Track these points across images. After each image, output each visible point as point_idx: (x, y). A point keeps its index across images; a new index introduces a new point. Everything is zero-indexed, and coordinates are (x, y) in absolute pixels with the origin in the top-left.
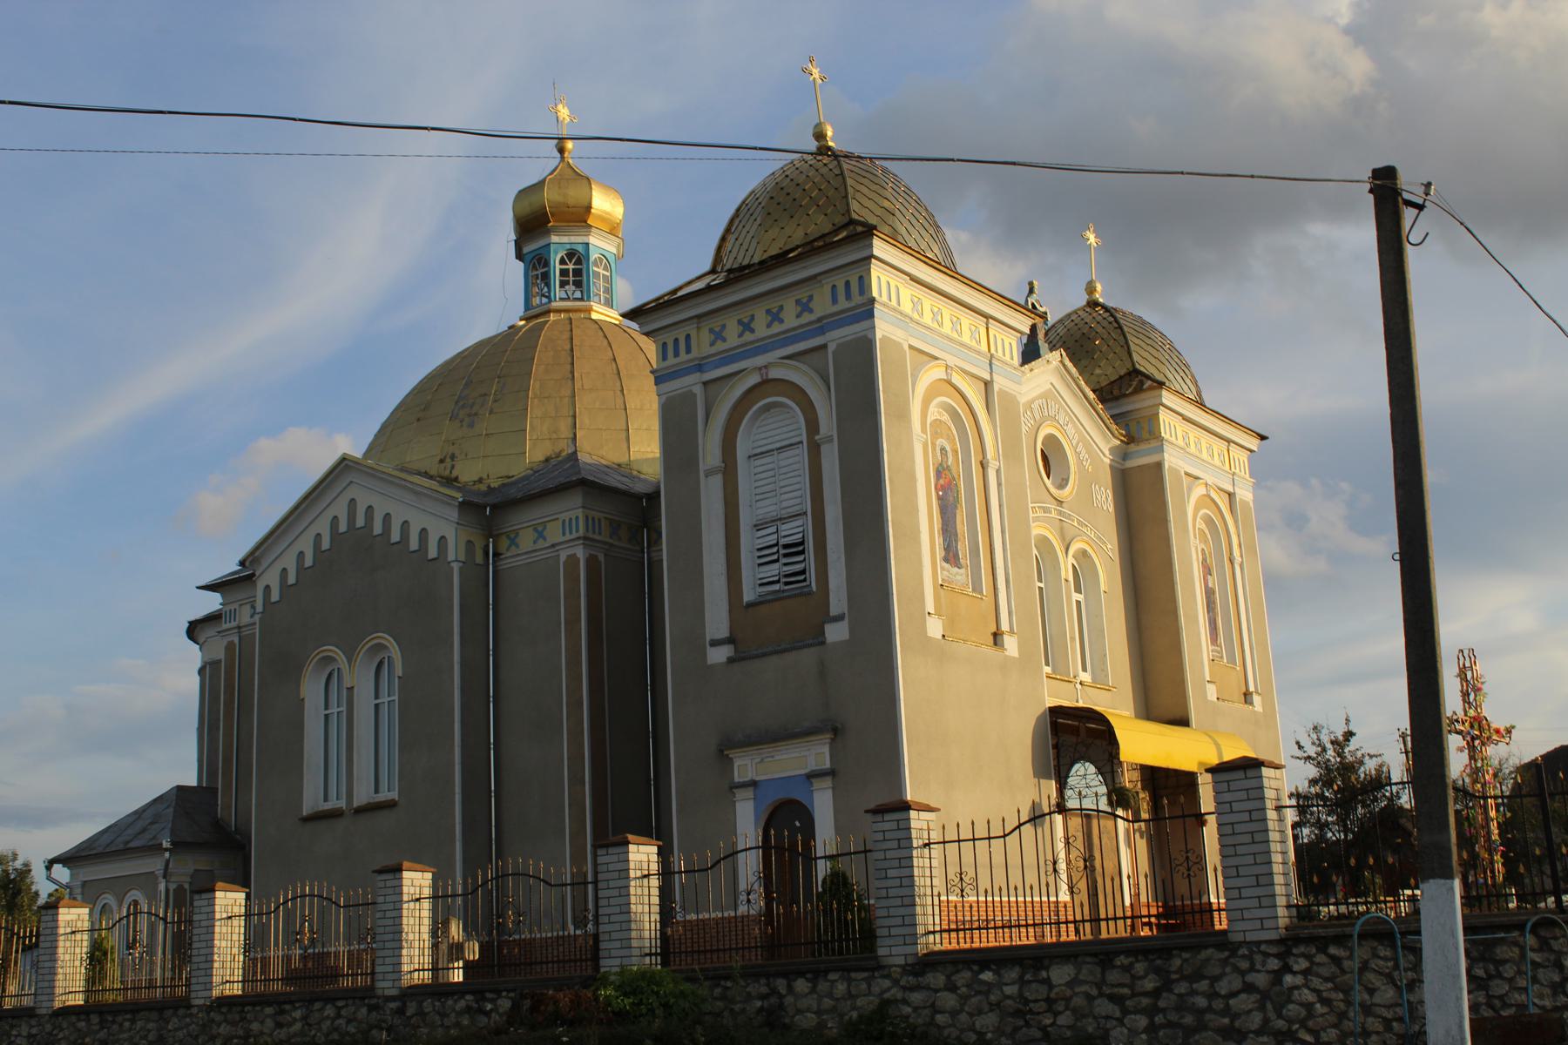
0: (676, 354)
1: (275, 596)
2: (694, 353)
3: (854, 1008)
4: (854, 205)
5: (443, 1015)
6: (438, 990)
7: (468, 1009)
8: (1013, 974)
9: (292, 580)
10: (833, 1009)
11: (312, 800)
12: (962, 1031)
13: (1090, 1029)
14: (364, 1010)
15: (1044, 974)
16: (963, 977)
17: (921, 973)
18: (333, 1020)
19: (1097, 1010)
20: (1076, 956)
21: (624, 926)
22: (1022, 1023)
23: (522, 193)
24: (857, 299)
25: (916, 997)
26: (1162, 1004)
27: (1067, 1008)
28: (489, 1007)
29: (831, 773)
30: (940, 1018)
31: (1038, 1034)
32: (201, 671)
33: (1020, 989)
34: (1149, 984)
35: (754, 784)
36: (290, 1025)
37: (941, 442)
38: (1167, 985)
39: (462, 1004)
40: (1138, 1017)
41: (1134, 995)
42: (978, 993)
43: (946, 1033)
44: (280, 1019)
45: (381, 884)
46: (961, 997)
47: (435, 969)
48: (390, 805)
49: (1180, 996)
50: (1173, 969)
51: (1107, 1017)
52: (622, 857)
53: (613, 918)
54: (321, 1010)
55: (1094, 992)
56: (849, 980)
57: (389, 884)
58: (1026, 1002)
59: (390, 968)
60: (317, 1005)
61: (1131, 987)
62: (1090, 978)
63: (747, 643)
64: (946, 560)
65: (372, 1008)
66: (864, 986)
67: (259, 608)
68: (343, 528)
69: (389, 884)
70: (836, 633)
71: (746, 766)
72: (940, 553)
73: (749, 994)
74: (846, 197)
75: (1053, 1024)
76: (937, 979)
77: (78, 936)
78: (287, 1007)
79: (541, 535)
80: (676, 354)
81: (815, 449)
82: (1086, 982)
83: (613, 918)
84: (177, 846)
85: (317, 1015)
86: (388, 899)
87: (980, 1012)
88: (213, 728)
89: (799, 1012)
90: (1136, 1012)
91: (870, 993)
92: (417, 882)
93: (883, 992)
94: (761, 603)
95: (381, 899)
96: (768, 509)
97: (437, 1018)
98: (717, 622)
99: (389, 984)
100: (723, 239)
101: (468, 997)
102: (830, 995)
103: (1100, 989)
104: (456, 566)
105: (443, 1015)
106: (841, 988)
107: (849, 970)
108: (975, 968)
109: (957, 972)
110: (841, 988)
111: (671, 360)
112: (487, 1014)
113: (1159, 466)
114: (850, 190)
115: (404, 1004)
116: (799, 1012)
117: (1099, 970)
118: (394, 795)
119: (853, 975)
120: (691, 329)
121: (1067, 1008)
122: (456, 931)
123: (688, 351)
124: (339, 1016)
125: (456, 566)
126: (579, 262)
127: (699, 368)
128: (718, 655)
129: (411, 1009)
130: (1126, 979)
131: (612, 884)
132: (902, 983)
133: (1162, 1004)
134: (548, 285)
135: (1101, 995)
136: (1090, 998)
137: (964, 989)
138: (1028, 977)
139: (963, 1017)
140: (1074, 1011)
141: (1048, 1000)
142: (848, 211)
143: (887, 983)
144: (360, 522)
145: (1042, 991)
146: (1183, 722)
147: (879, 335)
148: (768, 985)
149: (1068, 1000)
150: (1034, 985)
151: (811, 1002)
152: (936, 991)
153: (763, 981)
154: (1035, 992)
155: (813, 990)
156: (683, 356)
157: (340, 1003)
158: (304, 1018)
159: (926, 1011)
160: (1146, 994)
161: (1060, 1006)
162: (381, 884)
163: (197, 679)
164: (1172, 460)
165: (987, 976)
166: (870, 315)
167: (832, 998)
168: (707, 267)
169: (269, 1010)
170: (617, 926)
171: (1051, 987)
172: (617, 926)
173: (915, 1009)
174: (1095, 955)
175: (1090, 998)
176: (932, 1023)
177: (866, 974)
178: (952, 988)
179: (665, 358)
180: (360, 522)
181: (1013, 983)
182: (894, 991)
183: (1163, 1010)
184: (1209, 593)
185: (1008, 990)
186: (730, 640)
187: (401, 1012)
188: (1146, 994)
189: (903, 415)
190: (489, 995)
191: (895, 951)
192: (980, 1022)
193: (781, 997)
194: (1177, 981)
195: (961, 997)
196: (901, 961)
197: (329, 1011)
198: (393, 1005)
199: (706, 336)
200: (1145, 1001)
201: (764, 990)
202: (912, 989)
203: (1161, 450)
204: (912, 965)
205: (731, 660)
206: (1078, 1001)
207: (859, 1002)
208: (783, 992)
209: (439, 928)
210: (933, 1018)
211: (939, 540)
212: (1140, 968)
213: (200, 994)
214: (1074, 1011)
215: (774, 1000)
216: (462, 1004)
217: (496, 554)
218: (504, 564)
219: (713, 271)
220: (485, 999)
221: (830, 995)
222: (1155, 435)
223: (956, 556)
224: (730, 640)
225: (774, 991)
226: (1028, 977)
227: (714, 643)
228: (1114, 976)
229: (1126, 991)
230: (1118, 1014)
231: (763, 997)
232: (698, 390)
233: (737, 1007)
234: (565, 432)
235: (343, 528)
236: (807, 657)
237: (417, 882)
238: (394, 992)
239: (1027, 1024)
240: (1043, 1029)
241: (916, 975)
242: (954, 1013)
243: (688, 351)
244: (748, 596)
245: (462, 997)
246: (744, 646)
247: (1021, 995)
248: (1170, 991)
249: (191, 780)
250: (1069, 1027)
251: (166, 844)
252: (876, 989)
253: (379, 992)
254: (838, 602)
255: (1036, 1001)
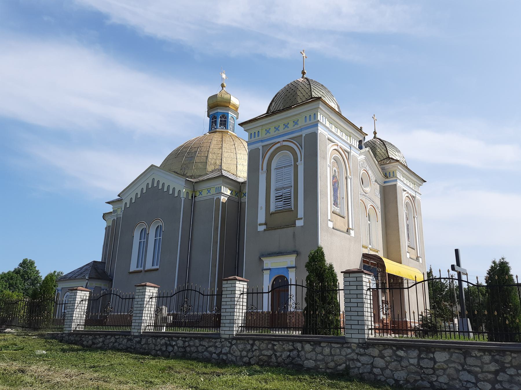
0: (255, 137)
1: (128, 206)
2: (260, 137)
3: (333, 361)
4: (313, 93)
5: (156, 345)
6: (155, 336)
7: (166, 344)
8: (415, 353)
9: (133, 201)
10: (323, 360)
11: (133, 268)
12: (387, 378)
13: (458, 386)
14: (125, 340)
15: (431, 355)
16: (388, 352)
17: (368, 348)
18: (114, 343)
19: (461, 378)
20: (449, 348)
21: (232, 314)
22: (419, 378)
23: (210, 99)
24: (313, 121)
25: (364, 359)
26: (499, 378)
27: (444, 374)
28: (174, 343)
29: (295, 267)
30: (375, 370)
31: (428, 385)
32: (106, 228)
33: (418, 362)
34: (493, 367)
35: (270, 269)
36: (98, 344)
37: (334, 168)
38: (503, 369)
39: (163, 341)
40: (486, 383)
41: (482, 372)
42: (395, 360)
43: (379, 378)
44: (94, 341)
45: (138, 291)
46: (386, 362)
47: (156, 326)
48: (157, 270)
49: (511, 376)
50: (507, 361)
51: (467, 382)
52: (233, 285)
53: (227, 310)
54: (110, 338)
55: (460, 368)
56: (331, 348)
57: (141, 291)
58: (422, 368)
59: (137, 324)
60: (109, 337)
61: (481, 368)
62: (457, 361)
63: (271, 226)
64: (334, 205)
65: (129, 340)
66: (338, 350)
67: (123, 209)
68: (150, 186)
69: (141, 291)
70: (299, 223)
71: (269, 263)
72: (333, 202)
73: (284, 348)
74: (311, 91)
75: (436, 381)
76: (375, 352)
77: (84, 302)
78: (97, 337)
79: (209, 192)
80: (255, 137)
81: (296, 167)
82: (454, 362)
83: (227, 310)
84: (90, 278)
85: (108, 341)
86: (140, 297)
87: (397, 370)
88: (107, 246)
89: (307, 359)
90: (484, 381)
91: (340, 355)
92: (151, 291)
93: (347, 355)
94: (275, 213)
95: (137, 297)
96: (280, 185)
97: (153, 346)
98: (262, 218)
99: (136, 331)
100: (271, 104)
101: (166, 339)
102: (321, 353)
103: (463, 366)
104: (183, 199)
105: (156, 345)
106: (327, 351)
107: (331, 343)
108: (394, 348)
109: (385, 349)
110: (327, 351)
111: (253, 139)
112: (173, 346)
113: (395, 185)
114: (312, 89)
115: (141, 339)
116: (307, 359)
117: (463, 357)
118: (158, 267)
119: (333, 345)
120: (259, 129)
121: (444, 374)
122: (165, 311)
123: (258, 136)
124: (116, 342)
125: (183, 199)
126: (226, 118)
127: (262, 141)
128: (261, 228)
129: (144, 341)
130: (479, 363)
131: (228, 296)
132: (357, 351)
133: (499, 378)
134: (216, 125)
135: (464, 369)
136: (458, 371)
137: (388, 358)
138: (422, 356)
139: (388, 372)
140: (448, 375)
141: (433, 368)
142: (311, 95)
143: (349, 351)
144: (155, 185)
145: (431, 364)
146: (401, 263)
147: (319, 132)
148: (293, 345)
149: (445, 370)
150: (426, 360)
151: (313, 355)
152: (374, 357)
153: (291, 343)
154: (425, 363)
155: (313, 350)
156: (257, 138)
157: (117, 337)
158: (103, 342)
159: (369, 366)
160: (490, 372)
161: (440, 372)
162: (138, 291)
163: (105, 230)
164: (399, 184)
165: (401, 353)
166: (317, 125)
167: (322, 355)
168: (265, 112)
169: (90, 337)
170: (229, 314)
171: (435, 362)
172: (229, 314)
173: (363, 364)
174: (460, 349)
175: (458, 371)
176: (371, 372)
177: (339, 346)
178: (382, 357)
179: (251, 138)
180: (155, 185)
181: (415, 358)
182: (353, 354)
183: (501, 382)
184: (408, 226)
185: (412, 361)
186: (266, 224)
187: (139, 342)
188: (490, 372)
189: (325, 158)
190: (174, 338)
191: (353, 336)
192: (397, 375)
193: (299, 351)
194: (509, 368)
195: (386, 362)
196: (357, 341)
197: (113, 339)
198: (136, 339)
199: (264, 132)
200: (490, 376)
201: (291, 347)
202: (361, 355)
203: (396, 180)
204: (362, 344)
205: (265, 230)
206: (451, 371)
207: (335, 358)
208: (300, 349)
209: (158, 310)
210: (372, 370)
211: (332, 198)
212: (487, 358)
213: (67, 329)
214: (448, 375)
215: (295, 352)
216: (163, 341)
217: (195, 197)
218: (196, 199)
219: (267, 113)
220: (173, 340)
221: (321, 353)
222: (394, 175)
223: (337, 203)
224: (266, 224)
225: (295, 349)
226: (422, 356)
227: (260, 225)
228: (470, 361)
229: (478, 369)
230: (474, 381)
231: (290, 351)
232: (261, 148)
233: (278, 354)
234: (218, 162)
235: (150, 186)
236: (290, 230)
237: (151, 291)
238: (137, 334)
239: (422, 379)
240: (431, 383)
241: (364, 348)
242: (382, 369)
243: (258, 136)
244: (272, 209)
245: (164, 339)
246: (270, 227)
247: (418, 364)
248: (505, 372)
249: (99, 259)
250: (445, 384)
251: (87, 278)
252: (344, 353)
253: (132, 334)
254: (301, 213)
255: (427, 368)
